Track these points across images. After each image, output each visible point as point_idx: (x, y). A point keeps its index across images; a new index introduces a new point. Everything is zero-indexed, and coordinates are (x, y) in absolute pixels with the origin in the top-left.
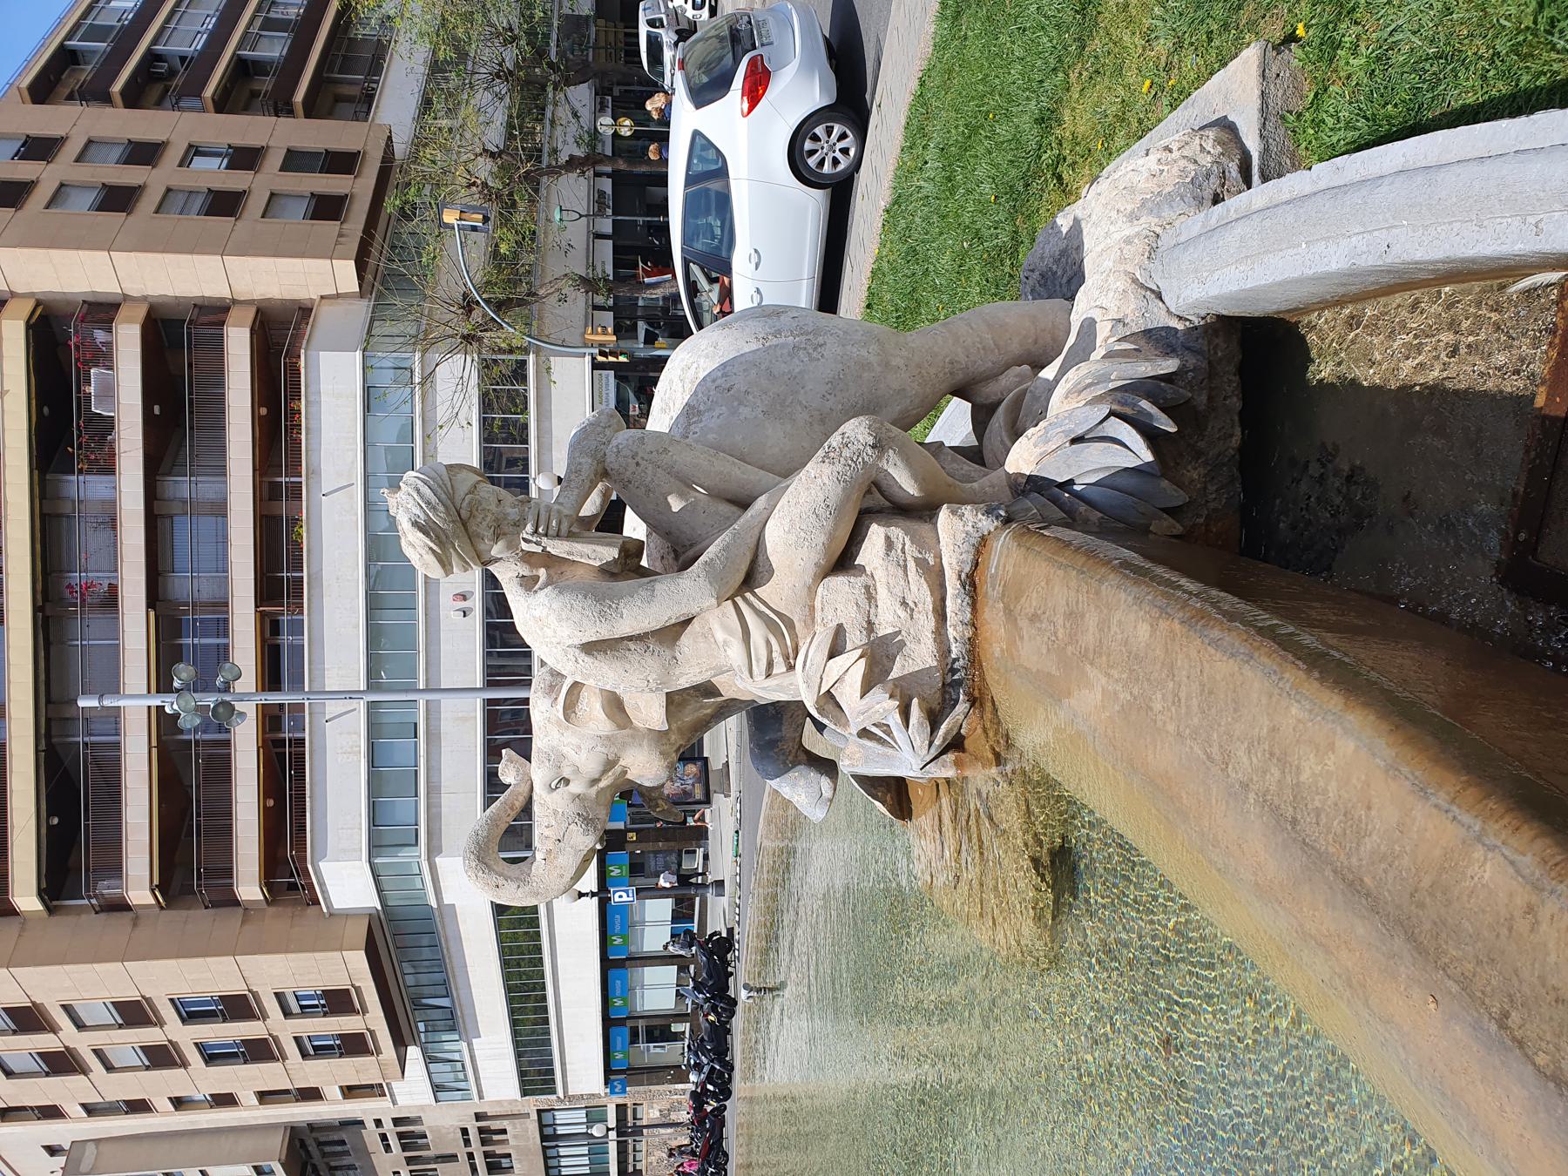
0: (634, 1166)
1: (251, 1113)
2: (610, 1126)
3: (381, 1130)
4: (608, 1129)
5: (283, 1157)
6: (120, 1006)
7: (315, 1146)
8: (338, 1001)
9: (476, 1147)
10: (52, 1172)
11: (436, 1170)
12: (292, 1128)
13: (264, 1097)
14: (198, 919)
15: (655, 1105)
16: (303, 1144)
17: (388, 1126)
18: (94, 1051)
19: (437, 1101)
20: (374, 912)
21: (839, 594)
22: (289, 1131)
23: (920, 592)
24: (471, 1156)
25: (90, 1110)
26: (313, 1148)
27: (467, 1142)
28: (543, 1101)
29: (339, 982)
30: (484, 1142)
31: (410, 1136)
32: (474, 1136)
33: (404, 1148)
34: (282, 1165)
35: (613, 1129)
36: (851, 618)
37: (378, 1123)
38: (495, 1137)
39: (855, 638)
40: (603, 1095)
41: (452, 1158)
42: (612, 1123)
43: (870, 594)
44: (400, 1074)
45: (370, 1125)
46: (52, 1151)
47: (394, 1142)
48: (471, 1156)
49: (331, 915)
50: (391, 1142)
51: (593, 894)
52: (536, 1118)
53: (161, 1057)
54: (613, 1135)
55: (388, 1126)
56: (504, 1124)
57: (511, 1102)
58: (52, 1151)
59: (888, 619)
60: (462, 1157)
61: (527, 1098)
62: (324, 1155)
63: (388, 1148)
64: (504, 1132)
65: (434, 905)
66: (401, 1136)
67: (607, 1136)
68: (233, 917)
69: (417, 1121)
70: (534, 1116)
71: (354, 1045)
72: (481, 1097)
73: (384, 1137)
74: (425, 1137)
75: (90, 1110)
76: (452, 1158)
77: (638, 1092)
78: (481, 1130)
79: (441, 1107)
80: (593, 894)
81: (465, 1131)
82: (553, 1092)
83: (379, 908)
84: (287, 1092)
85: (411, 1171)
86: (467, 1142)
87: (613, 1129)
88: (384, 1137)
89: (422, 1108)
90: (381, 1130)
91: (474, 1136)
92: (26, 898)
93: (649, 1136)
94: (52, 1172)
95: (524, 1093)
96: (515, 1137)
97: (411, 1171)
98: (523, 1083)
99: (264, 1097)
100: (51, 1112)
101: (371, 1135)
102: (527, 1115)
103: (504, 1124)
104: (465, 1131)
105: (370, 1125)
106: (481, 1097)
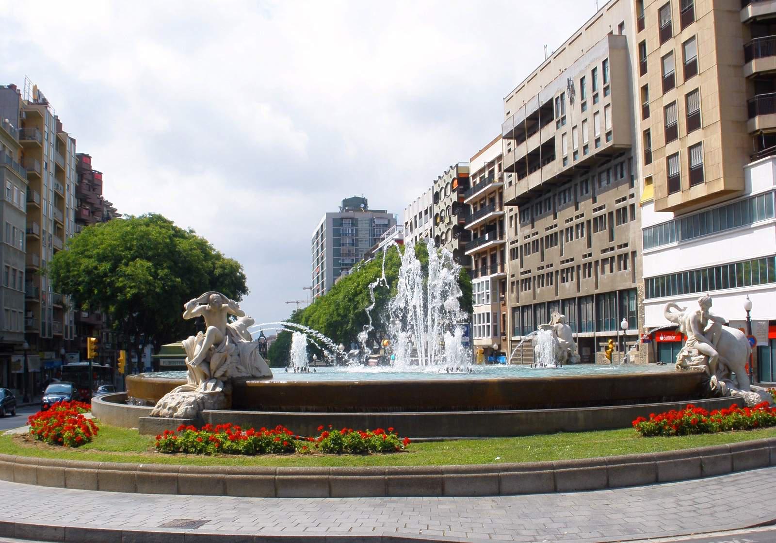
0: (603, 346)
1: (640, 126)
2: (626, 331)
3: (628, 197)
4: (625, 330)
5: (616, 146)
6: (695, 63)
7: (620, 161)
8: (697, 176)
9: (617, 252)
10: (610, 26)
11: (605, 229)
12: (631, 149)
13: (647, 134)
14: (740, 100)
15: (637, 358)
16: (621, 154)
17: (630, 201)
18: (672, 51)
19: (644, 229)
20: (747, 192)
21: (695, 352)
22: (628, 147)
23: (695, 363)
24: (612, 249)
25: (642, 46)
26: (620, 160)
27: (620, 247)
28: (641, 290)
29: (708, 175)
30: (620, 256)
31: (625, 214)
32: (623, 250)
33: (618, 211)
34: (611, 146)
35: (625, 333)
36: (693, 354)
37: (632, 196)
38: (622, 262)
39: (690, 354)
40: (644, 327)
41: (611, 238)
42: (629, 332)
43: (696, 356)
44: (658, 210)
45: (632, 191)
46: (621, 26)
47: (621, 205)
48: (612, 249)
49: (744, 169)
50: (621, 203)
51: (748, 318)
52: (633, 287)
53: (668, 83)
54: (621, 333)
55: (630, 201)
56: (629, 268)
57: (642, 274)
58: (621, 26)
59: (693, 359)
60: (612, 244)
61: (644, 281)
62: (616, 166)
63: (618, 201)
64: (625, 268)
65: (752, 226)
66: (625, 209)
67: (621, 329)
68: (743, 114)
69: (633, 217)
70: (633, 286)
71: (674, 185)
72: (645, 254)
73: (624, 199)
74: (624, 222)
75: (642, 46)
76: (611, 238)
77: (645, 348)
78: (626, 255)
79: (640, 231)
80: (748, 318)
81: (626, 245)
82: (647, 297)
83: (751, 195)
84: (650, 145)
85: (605, 215)
86: (620, 247)
87: (625, 333)
88: (624, 199)
89: (640, 220)
90: (628, 197)
91: (623, 250)
92: (751, 11)
93: (620, 355)
94: (610, 26)
95: (646, 280)
96: (622, 275)
97: (605, 215)
98: (652, 279)
99: (647, 134)
100: (641, 26)
101: (624, 190)
102: (634, 282)
103: (629, 268)
104: (626, 245)
105: (632, 191)
106: (645, 254)
